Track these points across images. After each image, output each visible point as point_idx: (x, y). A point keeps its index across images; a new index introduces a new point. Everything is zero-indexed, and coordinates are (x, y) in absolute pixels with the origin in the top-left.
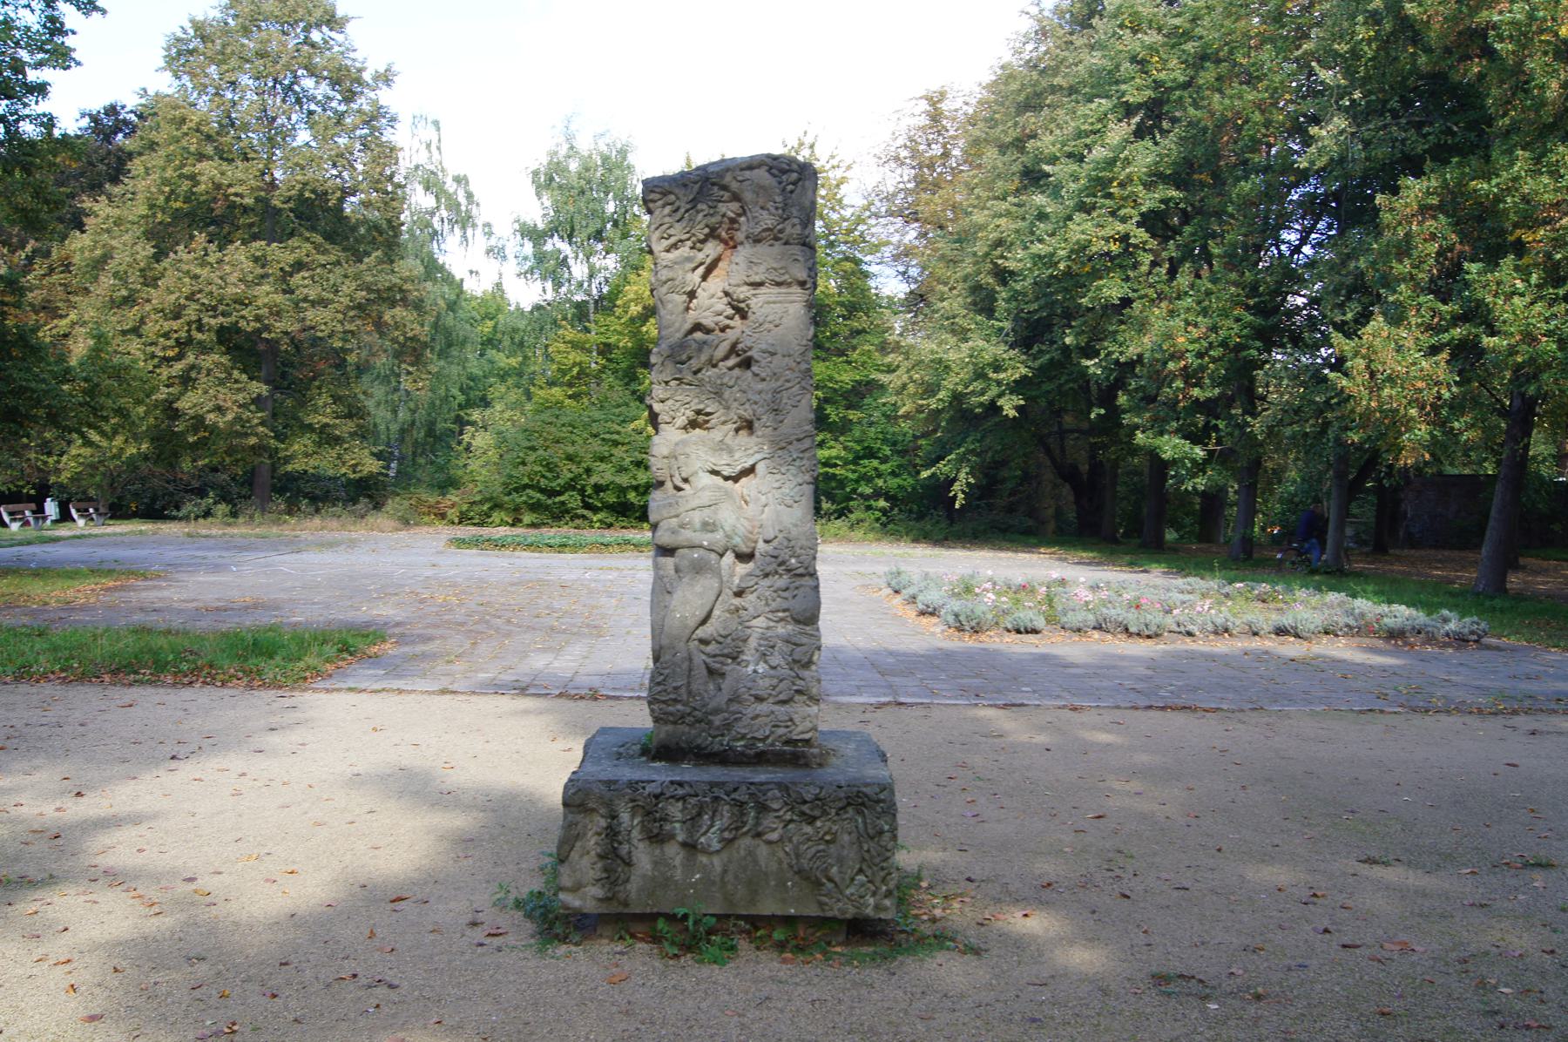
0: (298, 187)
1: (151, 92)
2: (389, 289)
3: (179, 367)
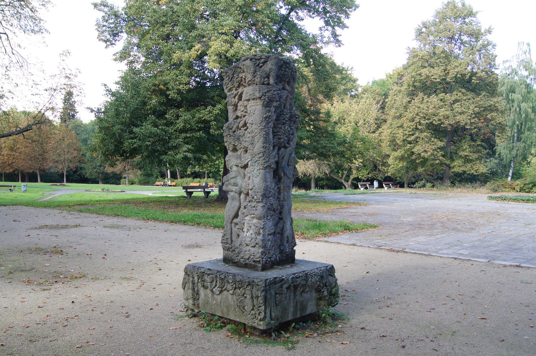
0: (456, 73)
1: (411, 48)
3: (413, 138)
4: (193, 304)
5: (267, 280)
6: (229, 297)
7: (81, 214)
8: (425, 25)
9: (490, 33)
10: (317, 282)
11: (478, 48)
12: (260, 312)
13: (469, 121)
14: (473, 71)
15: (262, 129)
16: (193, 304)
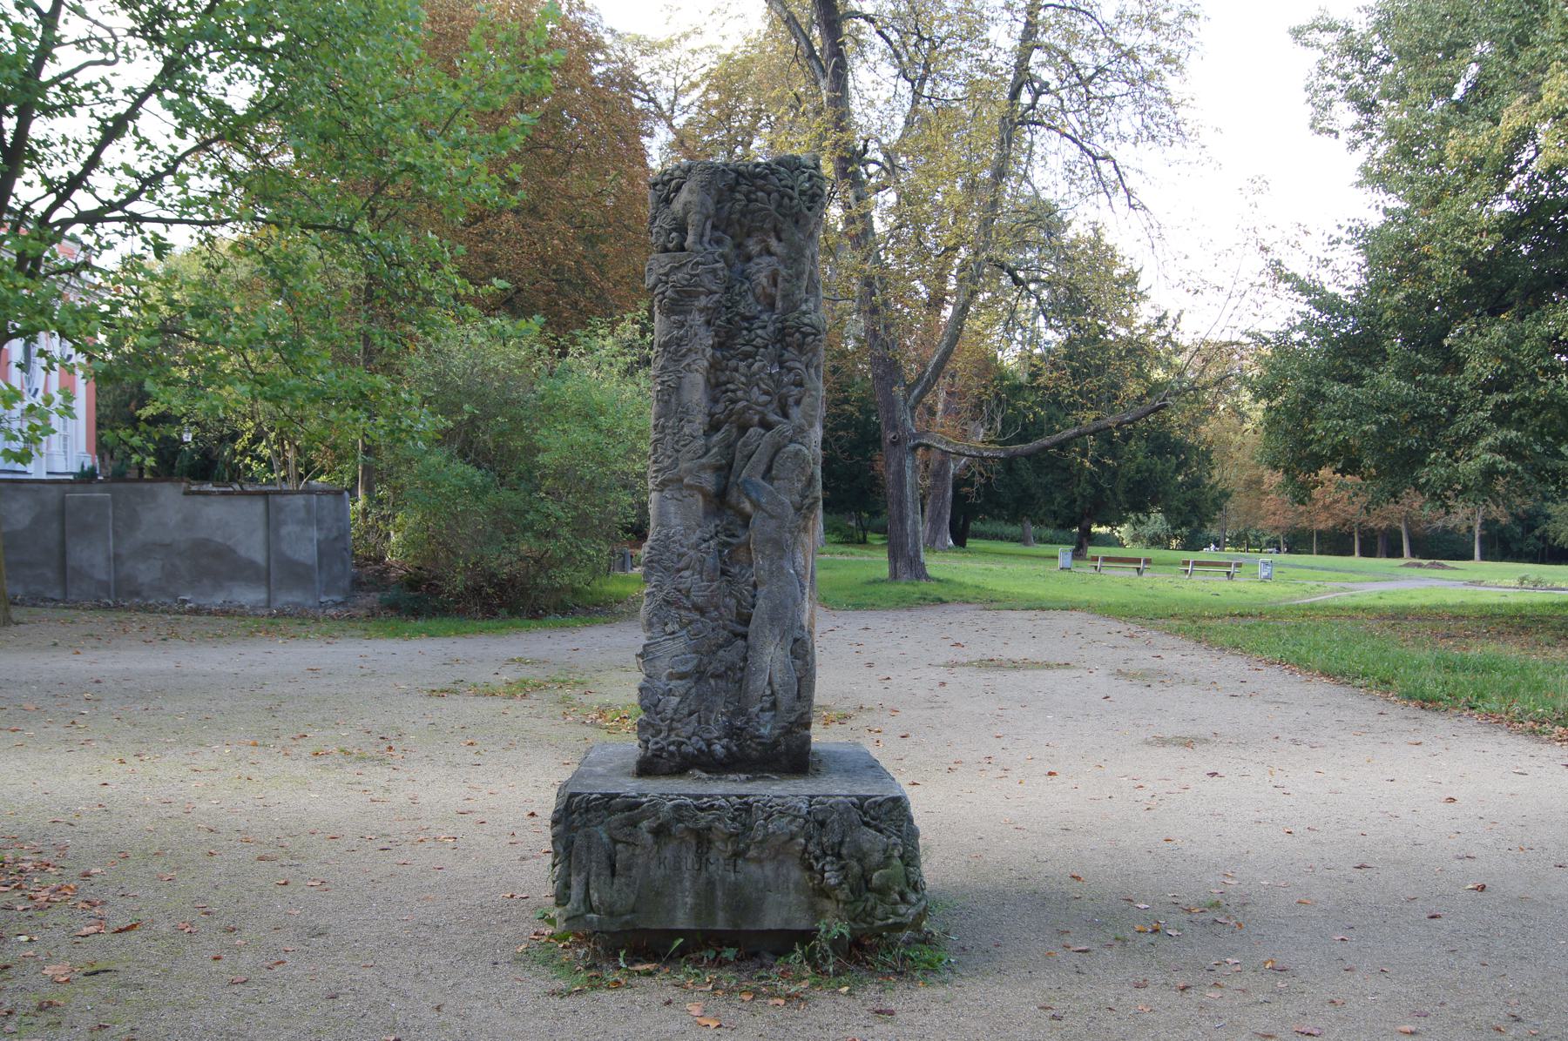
10: (793, 837)
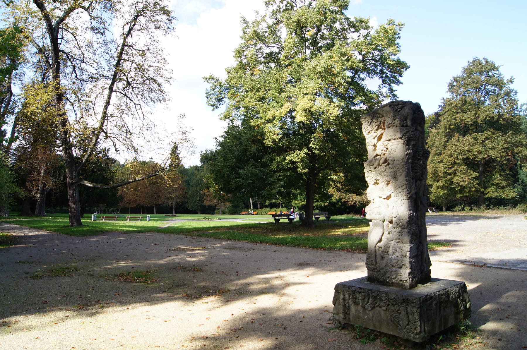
2: (516, 142)
3: (452, 170)
4: (344, 319)
5: (421, 297)
6: (382, 312)
7: (201, 238)
8: (456, 80)
9: (512, 83)
11: (502, 95)
12: (416, 327)
13: (499, 155)
14: (499, 114)
15: (404, 164)
16: (344, 319)
